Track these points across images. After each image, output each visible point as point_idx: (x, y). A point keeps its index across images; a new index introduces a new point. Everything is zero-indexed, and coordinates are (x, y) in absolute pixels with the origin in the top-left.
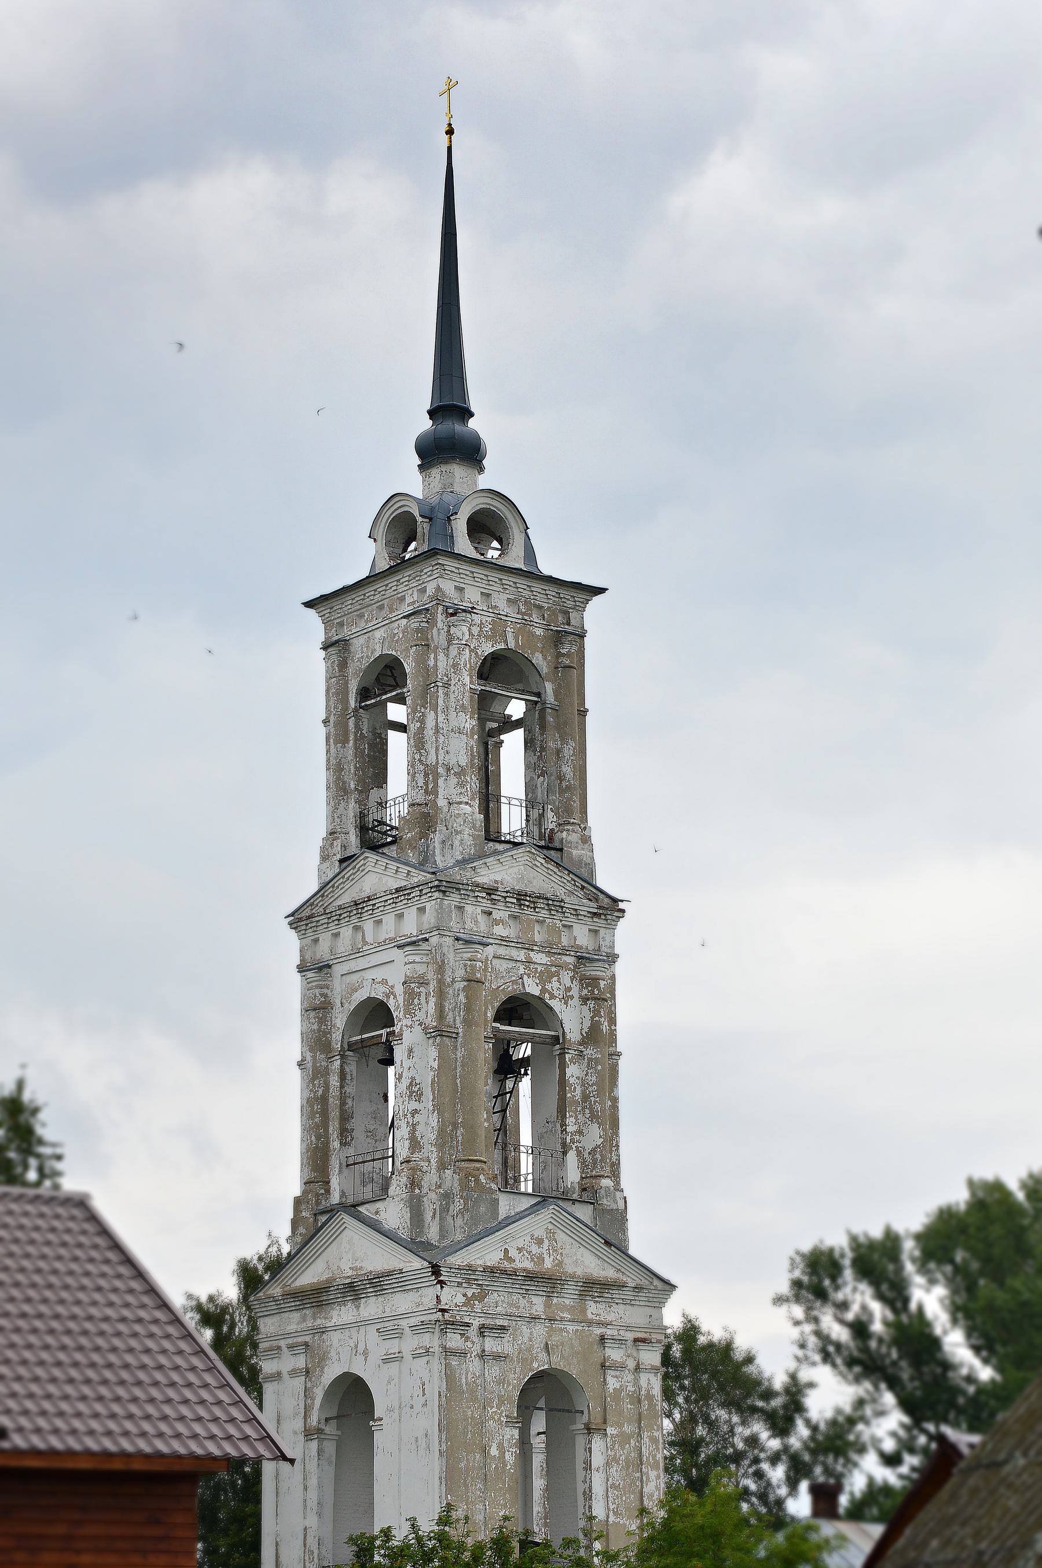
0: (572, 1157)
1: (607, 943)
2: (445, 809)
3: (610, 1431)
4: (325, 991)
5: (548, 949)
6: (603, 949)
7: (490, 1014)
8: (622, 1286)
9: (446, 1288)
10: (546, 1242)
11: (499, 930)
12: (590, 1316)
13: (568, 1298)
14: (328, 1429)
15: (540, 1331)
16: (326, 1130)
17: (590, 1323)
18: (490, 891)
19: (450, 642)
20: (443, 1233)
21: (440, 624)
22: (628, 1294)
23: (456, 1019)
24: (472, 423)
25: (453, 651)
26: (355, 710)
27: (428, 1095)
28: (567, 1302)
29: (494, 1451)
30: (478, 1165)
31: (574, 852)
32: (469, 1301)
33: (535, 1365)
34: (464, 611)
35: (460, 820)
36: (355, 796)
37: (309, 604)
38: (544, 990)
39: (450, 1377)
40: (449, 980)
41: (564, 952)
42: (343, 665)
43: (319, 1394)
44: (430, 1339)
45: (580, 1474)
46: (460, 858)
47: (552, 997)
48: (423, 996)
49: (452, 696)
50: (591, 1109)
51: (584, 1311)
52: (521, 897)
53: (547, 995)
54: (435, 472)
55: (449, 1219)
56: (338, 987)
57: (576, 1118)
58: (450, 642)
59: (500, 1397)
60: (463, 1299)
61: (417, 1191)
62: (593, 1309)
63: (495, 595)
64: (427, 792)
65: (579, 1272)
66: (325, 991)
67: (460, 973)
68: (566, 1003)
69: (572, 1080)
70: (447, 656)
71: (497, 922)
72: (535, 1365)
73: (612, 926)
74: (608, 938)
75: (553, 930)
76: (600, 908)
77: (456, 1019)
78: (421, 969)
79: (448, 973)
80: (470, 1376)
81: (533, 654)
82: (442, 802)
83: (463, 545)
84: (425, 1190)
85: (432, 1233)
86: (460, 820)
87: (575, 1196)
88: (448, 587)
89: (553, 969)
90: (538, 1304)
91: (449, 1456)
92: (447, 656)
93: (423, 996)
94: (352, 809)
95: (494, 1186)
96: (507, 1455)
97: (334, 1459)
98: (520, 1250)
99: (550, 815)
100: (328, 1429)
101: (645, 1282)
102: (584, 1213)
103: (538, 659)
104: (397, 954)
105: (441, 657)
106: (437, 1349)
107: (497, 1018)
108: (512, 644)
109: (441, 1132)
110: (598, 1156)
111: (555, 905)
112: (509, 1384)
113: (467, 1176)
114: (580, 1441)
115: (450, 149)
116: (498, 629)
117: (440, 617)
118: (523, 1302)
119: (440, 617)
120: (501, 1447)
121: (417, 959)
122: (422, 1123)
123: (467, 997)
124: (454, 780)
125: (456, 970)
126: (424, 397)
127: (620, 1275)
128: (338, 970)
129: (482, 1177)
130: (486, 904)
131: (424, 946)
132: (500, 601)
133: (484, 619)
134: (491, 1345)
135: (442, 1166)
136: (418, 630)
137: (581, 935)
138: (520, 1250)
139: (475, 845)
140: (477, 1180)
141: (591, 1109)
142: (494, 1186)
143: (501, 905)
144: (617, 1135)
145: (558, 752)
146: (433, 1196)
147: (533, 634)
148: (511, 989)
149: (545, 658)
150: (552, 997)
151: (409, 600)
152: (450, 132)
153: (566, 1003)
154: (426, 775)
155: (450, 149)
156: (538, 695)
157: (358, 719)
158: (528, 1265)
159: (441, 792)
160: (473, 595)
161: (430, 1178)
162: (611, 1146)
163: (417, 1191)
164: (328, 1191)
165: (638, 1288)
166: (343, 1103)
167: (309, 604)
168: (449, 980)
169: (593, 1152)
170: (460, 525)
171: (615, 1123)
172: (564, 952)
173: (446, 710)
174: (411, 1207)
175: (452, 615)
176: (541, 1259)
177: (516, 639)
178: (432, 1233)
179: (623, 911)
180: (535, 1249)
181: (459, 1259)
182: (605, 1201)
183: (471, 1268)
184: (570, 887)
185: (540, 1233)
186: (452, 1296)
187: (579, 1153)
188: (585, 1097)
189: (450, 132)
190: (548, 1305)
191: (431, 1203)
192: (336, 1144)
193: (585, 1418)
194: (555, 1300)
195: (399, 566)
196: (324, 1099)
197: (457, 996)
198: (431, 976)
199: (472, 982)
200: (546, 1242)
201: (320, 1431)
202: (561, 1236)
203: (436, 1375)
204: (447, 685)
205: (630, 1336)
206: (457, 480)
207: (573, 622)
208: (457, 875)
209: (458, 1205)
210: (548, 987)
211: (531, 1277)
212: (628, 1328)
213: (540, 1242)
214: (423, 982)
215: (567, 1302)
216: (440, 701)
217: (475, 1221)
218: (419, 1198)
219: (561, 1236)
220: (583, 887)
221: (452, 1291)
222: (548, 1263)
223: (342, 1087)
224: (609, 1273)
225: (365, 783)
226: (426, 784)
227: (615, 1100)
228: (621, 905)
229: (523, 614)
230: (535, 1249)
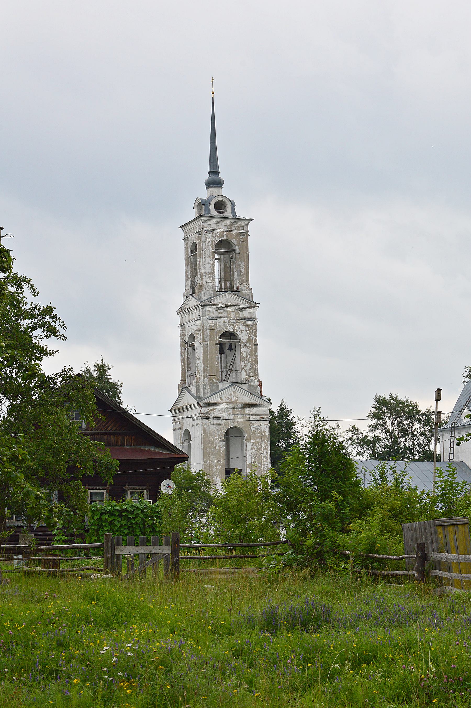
0: (243, 372)
1: (254, 315)
2: (205, 284)
3: (252, 441)
4: (184, 331)
5: (235, 318)
6: (253, 317)
7: (218, 337)
8: (255, 404)
9: (203, 408)
10: (233, 395)
11: (220, 315)
12: (246, 413)
13: (240, 408)
14: (185, 443)
15: (231, 417)
16: (185, 367)
17: (246, 414)
18: (217, 305)
19: (206, 239)
20: (204, 395)
21: (203, 235)
22: (257, 406)
23: (207, 339)
24: (220, 175)
25: (207, 242)
26: (190, 257)
27: (201, 359)
28: (239, 409)
29: (217, 448)
30: (213, 376)
31: (244, 292)
32: (210, 411)
33: (230, 426)
34: (209, 231)
35: (209, 287)
36: (190, 279)
37: (180, 227)
38: (234, 329)
39: (204, 430)
40: (205, 329)
41: (240, 319)
42: (187, 244)
43: (182, 433)
44: (199, 421)
45: (245, 451)
46: (209, 297)
47: (237, 331)
48: (199, 334)
49: (207, 254)
50: (248, 359)
51: (244, 412)
52: (226, 306)
53: (235, 331)
54: (209, 190)
55: (206, 391)
56: (186, 330)
57: (244, 362)
58: (206, 239)
59: (219, 434)
60: (208, 411)
61: (198, 384)
62: (247, 411)
63: (220, 225)
64: (201, 280)
65: (243, 402)
66: (184, 331)
67: (208, 327)
68: (241, 332)
69: (243, 352)
70: (206, 243)
71: (220, 313)
72: (230, 426)
73: (255, 310)
74: (254, 314)
75: (237, 313)
76: (251, 306)
77: (207, 339)
78: (199, 327)
79: (205, 327)
80: (210, 429)
81: (232, 239)
82: (204, 283)
83: (214, 212)
84: (200, 384)
85: (202, 395)
86: (209, 287)
87: (244, 382)
88: (206, 225)
89: (237, 324)
90: (230, 411)
91: (204, 450)
92: (206, 243)
93: (199, 334)
94: (190, 283)
95: (217, 382)
96: (221, 449)
97: (187, 450)
98: (225, 397)
99: (238, 282)
100: (185, 443)
101: (262, 403)
102: (245, 387)
103: (234, 241)
104: (194, 323)
105: (204, 244)
106: (201, 424)
107: (220, 338)
108: (225, 238)
109: (204, 368)
110: (250, 371)
111: (237, 306)
112: (222, 431)
113: (210, 379)
114: (245, 443)
115: (213, 98)
116: (221, 233)
117: (203, 233)
118: (226, 410)
119: (203, 233)
120: (219, 447)
121: (198, 324)
122: (200, 366)
123: (210, 334)
124: (207, 276)
125: (207, 326)
126: (206, 168)
127: (256, 402)
128: (186, 326)
129: (214, 380)
130: (217, 309)
131: (199, 321)
132: (222, 226)
133: (217, 232)
134: (216, 421)
135: (204, 377)
136: (198, 237)
137: (246, 314)
138: (225, 397)
139: (213, 293)
140: (212, 380)
141: (248, 359)
142: (217, 382)
143: (221, 308)
144: (257, 365)
145: (240, 265)
146: (202, 385)
147: (232, 234)
148: (224, 330)
149: (236, 240)
150: (237, 331)
151: (198, 228)
152: (213, 93)
153: (241, 332)
154: (201, 275)
155: (213, 98)
156: (235, 250)
157: (191, 259)
158: (228, 401)
159: (204, 280)
160: (213, 226)
161: (201, 381)
162: (255, 368)
163: (198, 384)
164: (185, 383)
165: (260, 405)
166: (188, 360)
167: (180, 227)
168: (205, 329)
169: (249, 370)
170: (212, 206)
171: (256, 362)
172: (240, 319)
173: (205, 258)
174: (196, 388)
175: (206, 232)
176: (231, 399)
177: (227, 236)
178: (202, 395)
179: (258, 306)
180: (229, 397)
181: (206, 401)
182: (251, 383)
183: (209, 403)
184: (242, 301)
185: (231, 392)
186: (204, 410)
187: (245, 371)
188: (247, 356)
189: (213, 93)
190: (233, 411)
191: (201, 387)
192: (187, 371)
193: (245, 438)
194: (236, 409)
195: (200, 216)
196: (184, 359)
197: (208, 334)
198: (201, 329)
199: (212, 330)
200: (233, 395)
201: (183, 443)
202: (237, 393)
203: (200, 430)
204: (205, 251)
205: (258, 417)
206: (214, 192)
207: (245, 229)
208: (207, 302)
209: (208, 387)
210: (236, 328)
211: (227, 404)
212: (258, 415)
213: (231, 395)
214: (199, 331)
215: (239, 409)
216: (204, 256)
217: (211, 391)
218: (199, 385)
219: (237, 393)
220: (246, 301)
221: (205, 409)
222: (233, 400)
223: (188, 356)
224: (253, 401)
225: (193, 275)
226: (201, 278)
227: (257, 356)
228: (258, 305)
229: (229, 229)
230: (229, 397)
